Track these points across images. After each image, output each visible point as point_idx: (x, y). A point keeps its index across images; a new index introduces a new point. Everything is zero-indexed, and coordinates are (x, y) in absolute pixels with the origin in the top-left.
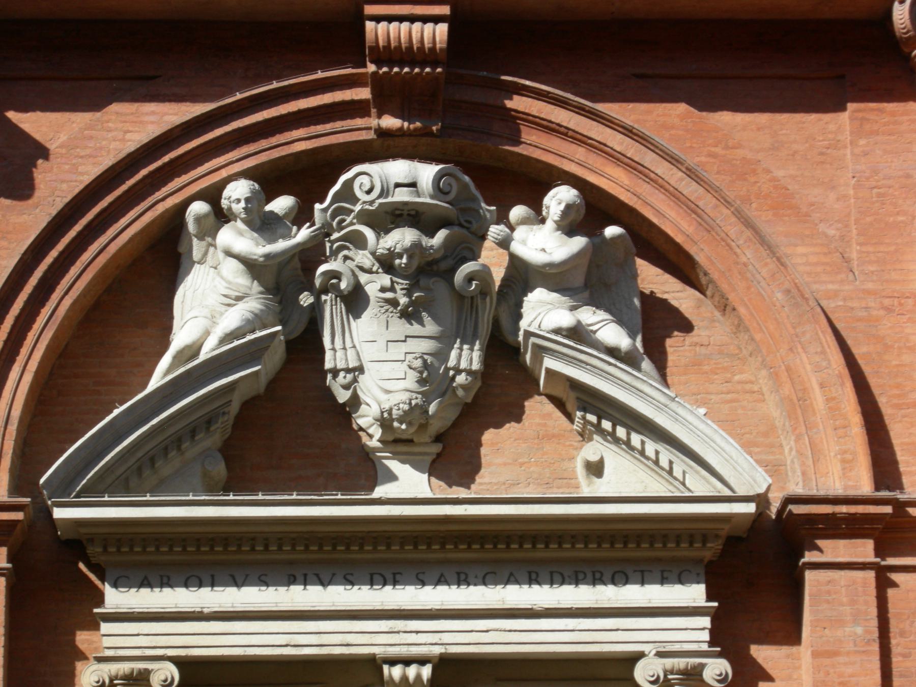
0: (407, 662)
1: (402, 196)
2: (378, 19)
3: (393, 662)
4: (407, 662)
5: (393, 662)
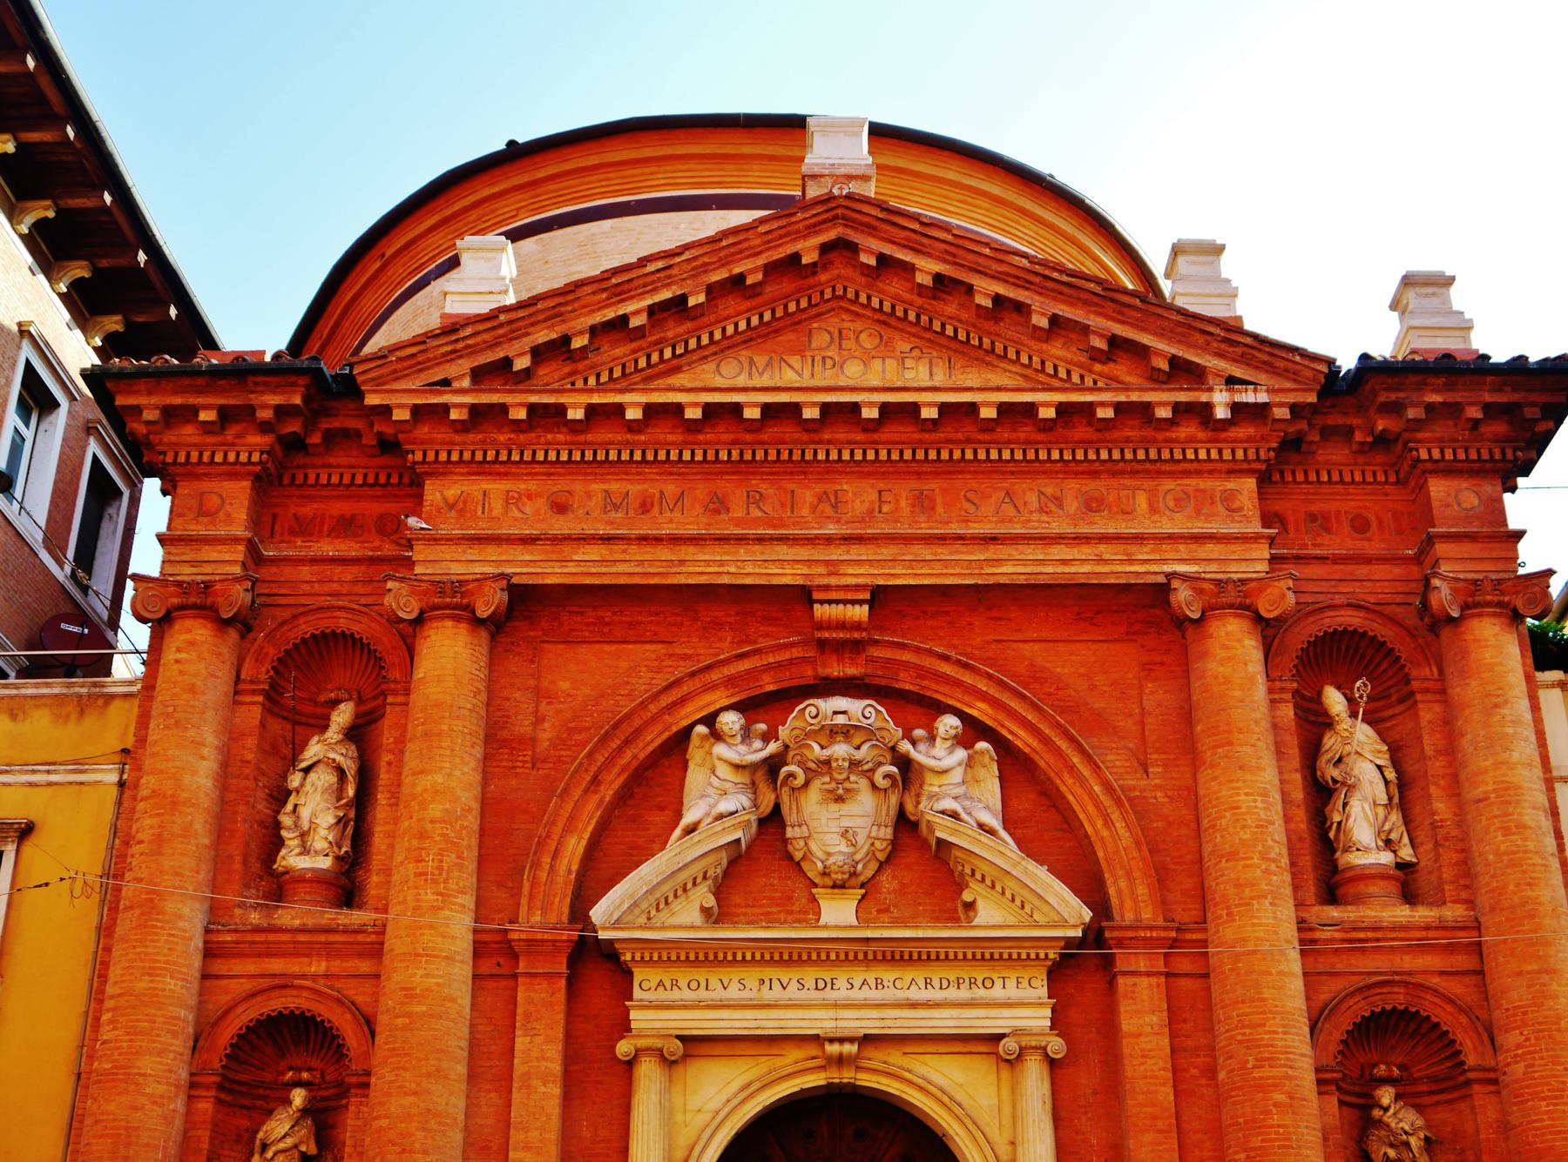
0: (841, 1040)
1: (841, 720)
2: (822, 602)
3: (831, 1041)
4: (841, 1040)
5: (831, 1041)
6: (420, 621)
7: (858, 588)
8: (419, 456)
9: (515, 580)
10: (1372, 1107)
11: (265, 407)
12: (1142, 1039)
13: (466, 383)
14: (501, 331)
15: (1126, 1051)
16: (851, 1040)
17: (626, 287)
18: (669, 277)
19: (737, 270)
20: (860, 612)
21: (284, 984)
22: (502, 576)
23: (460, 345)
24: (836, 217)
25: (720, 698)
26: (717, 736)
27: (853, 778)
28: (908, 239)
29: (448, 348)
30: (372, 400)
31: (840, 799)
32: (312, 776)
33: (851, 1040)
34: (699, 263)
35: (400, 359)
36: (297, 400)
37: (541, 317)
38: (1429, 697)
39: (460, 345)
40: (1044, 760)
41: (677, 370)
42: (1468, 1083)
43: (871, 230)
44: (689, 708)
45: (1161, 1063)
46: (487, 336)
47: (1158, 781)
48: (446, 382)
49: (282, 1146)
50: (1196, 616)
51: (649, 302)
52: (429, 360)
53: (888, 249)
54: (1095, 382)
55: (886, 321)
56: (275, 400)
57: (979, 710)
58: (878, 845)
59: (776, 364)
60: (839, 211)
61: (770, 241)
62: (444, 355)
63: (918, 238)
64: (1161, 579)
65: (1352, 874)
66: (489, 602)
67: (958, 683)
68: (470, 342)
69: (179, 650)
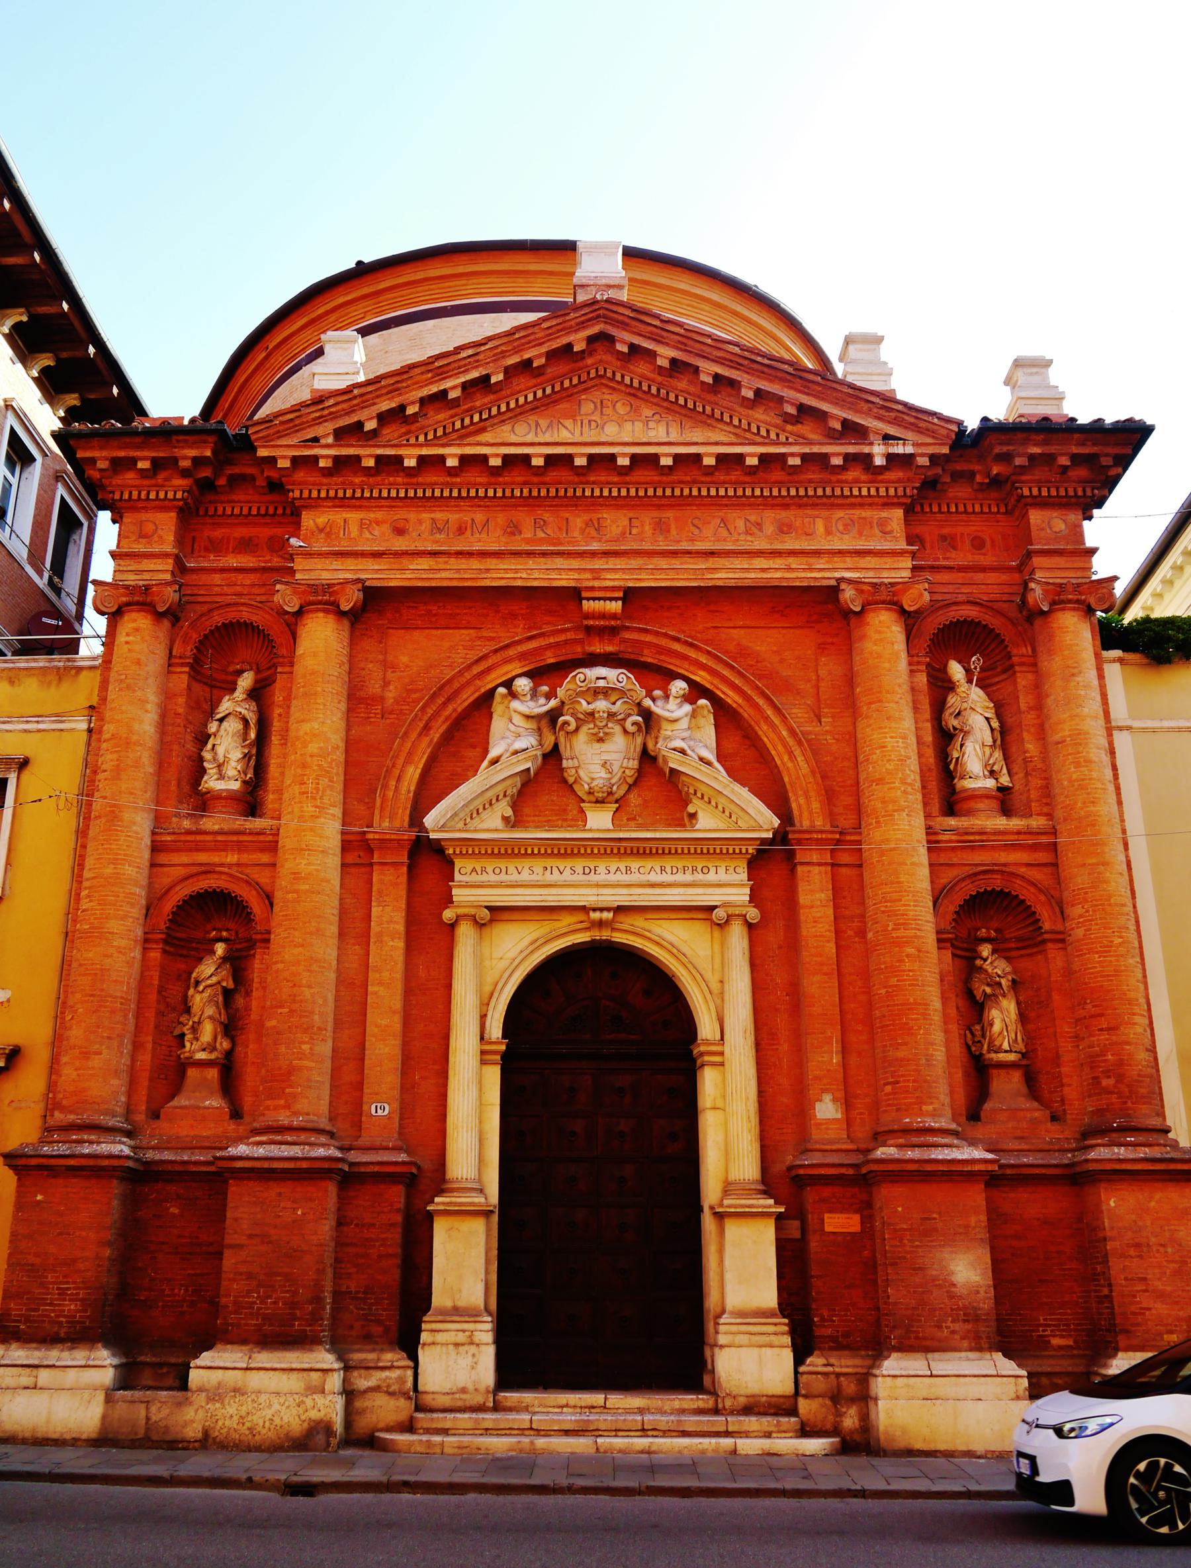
0: (601, 910)
1: (601, 683)
2: (588, 599)
3: (594, 910)
4: (601, 910)
5: (594, 910)
6: (300, 613)
7: (614, 589)
8: (297, 494)
9: (367, 584)
10: (975, 958)
11: (185, 458)
12: (814, 910)
13: (330, 440)
14: (355, 402)
15: (802, 918)
16: (608, 909)
17: (445, 369)
18: (477, 361)
19: (526, 356)
20: (616, 606)
21: (208, 870)
22: (358, 580)
23: (326, 412)
24: (599, 316)
25: (515, 668)
26: (513, 695)
27: (610, 725)
28: (651, 333)
29: (317, 415)
30: (262, 452)
31: (601, 740)
32: (225, 724)
33: (608, 909)
34: (499, 350)
35: (282, 423)
36: (208, 453)
37: (384, 391)
38: (1024, 668)
39: (326, 412)
40: (747, 712)
41: (483, 430)
42: (1044, 941)
43: (624, 326)
44: (493, 675)
45: (827, 927)
46: (345, 406)
47: (827, 728)
48: (316, 440)
49: (209, 982)
50: (858, 609)
51: (463, 380)
52: (303, 423)
53: (637, 340)
54: (787, 439)
55: (635, 393)
56: (193, 453)
57: (701, 677)
58: (628, 772)
59: (555, 426)
60: (601, 312)
61: (551, 334)
62: (314, 419)
63: (659, 331)
64: (833, 583)
65: (965, 794)
66: (350, 599)
67: (685, 658)
68: (332, 410)
69: (128, 635)
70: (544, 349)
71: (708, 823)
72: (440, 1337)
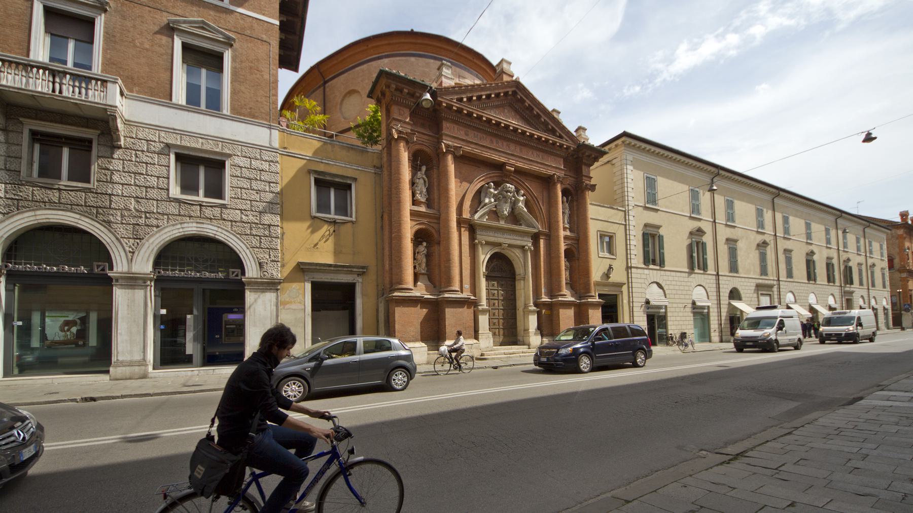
30: (439, 99)
55: (516, 111)
67: (521, 185)
70: (503, 90)
71: (523, 228)
72: (484, 337)
